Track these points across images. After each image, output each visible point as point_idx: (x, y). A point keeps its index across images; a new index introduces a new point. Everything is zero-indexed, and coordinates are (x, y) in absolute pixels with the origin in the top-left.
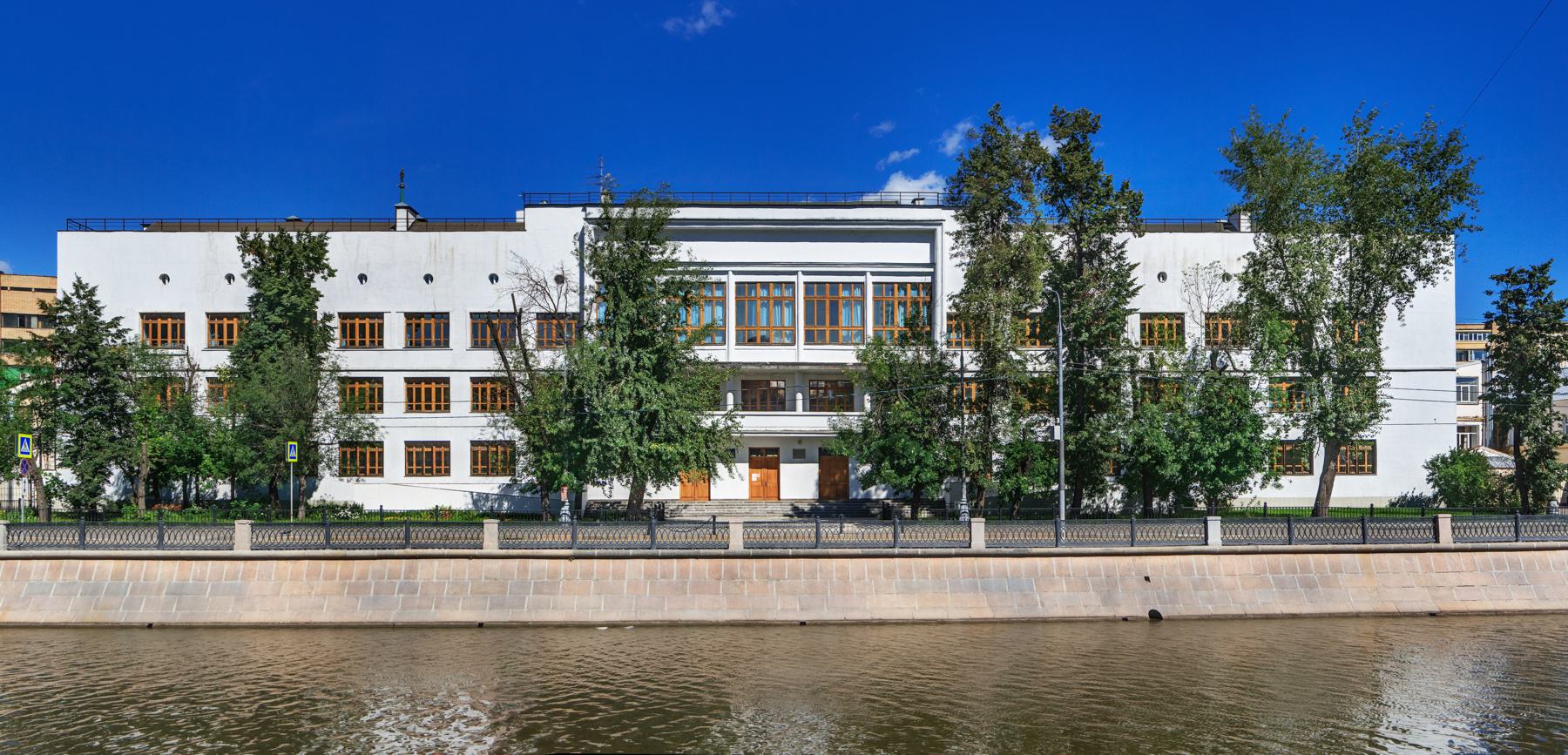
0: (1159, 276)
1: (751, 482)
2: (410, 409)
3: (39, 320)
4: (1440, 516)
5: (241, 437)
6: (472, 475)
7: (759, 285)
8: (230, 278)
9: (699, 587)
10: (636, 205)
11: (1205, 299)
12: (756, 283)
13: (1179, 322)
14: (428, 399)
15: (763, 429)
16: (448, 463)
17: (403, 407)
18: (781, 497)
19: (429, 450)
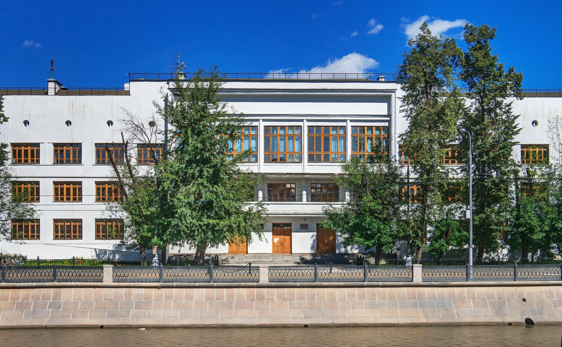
2: (56, 200)
6: (96, 239)
12: (277, 126)
13: (545, 150)
14: (68, 193)
18: (49, 83)
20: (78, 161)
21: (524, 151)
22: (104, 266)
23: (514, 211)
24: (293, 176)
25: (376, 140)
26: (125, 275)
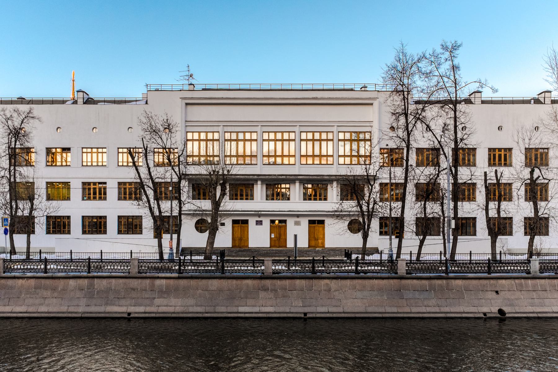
1: (271, 238)
3: (262, 182)
5: (205, 259)
6: (118, 234)
7: (425, 150)
9: (165, 293)
10: (246, 270)
11: (527, 141)
16: (105, 194)
20: (501, 154)
21: (140, 228)
23: (238, 350)
24: (288, 177)
25: (237, 285)
26: (366, 163)
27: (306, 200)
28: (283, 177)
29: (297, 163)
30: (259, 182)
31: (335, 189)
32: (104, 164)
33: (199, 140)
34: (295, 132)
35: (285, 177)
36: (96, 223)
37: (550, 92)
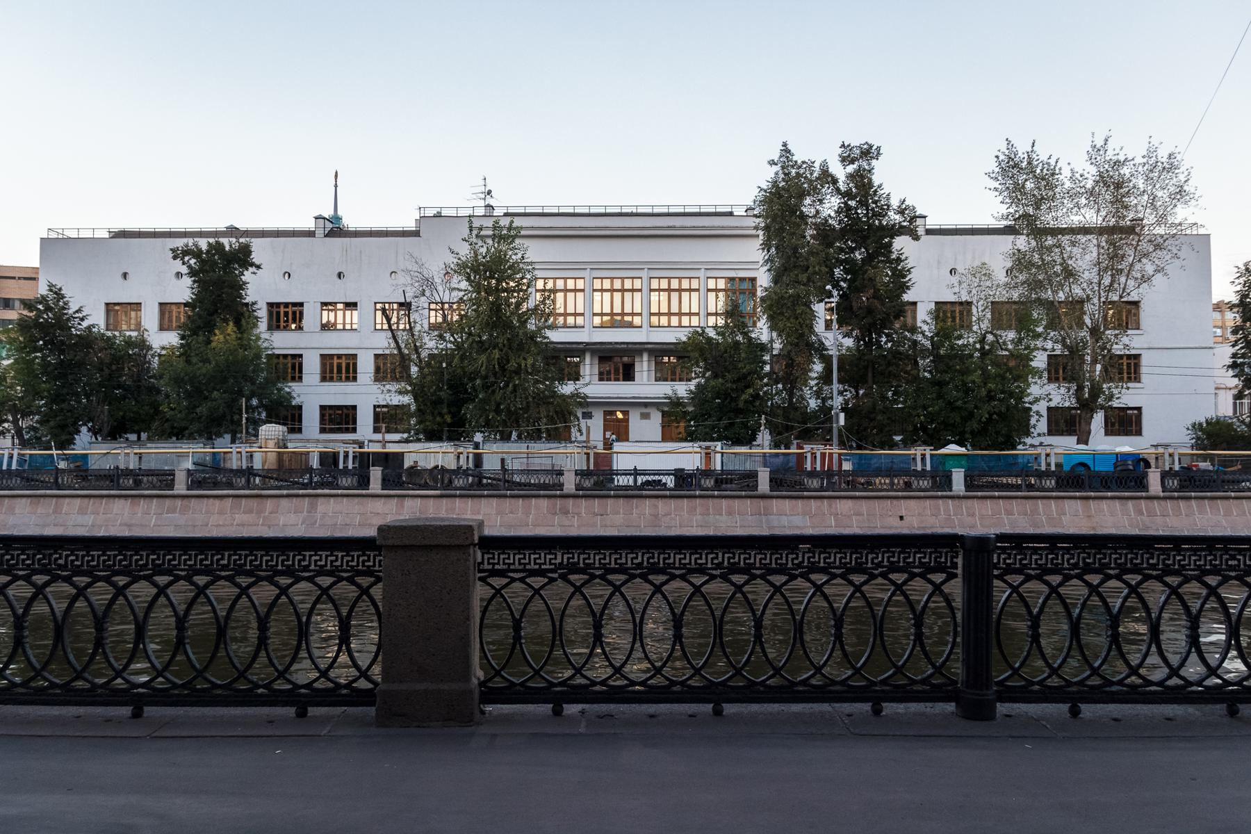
0: (951, 272)
2: (324, 379)
4: (953, 470)
8: (1114, 150)
14: (339, 371)
15: (616, 396)
17: (318, 377)
19: (340, 412)
20: (288, 312)
22: (953, 470)
27: (675, 381)
28: (623, 346)
29: (645, 325)
30: (645, 357)
31: (645, 364)
32: (355, 327)
33: (612, 291)
34: (641, 278)
35: (625, 346)
36: (341, 415)
37: (925, 217)
